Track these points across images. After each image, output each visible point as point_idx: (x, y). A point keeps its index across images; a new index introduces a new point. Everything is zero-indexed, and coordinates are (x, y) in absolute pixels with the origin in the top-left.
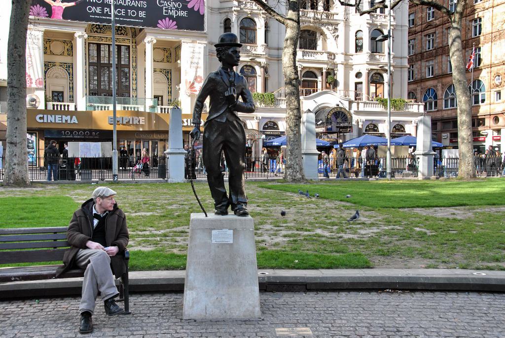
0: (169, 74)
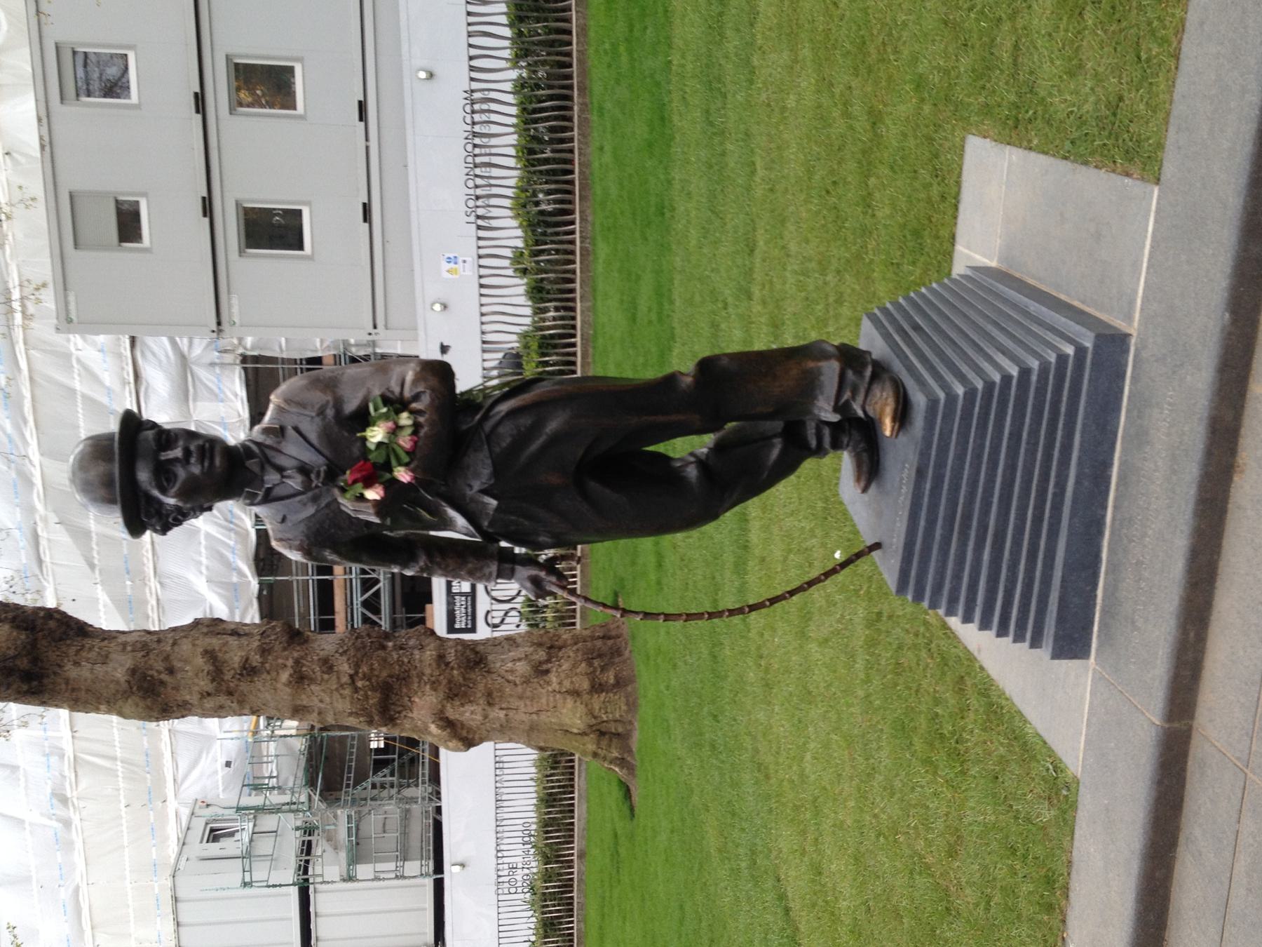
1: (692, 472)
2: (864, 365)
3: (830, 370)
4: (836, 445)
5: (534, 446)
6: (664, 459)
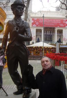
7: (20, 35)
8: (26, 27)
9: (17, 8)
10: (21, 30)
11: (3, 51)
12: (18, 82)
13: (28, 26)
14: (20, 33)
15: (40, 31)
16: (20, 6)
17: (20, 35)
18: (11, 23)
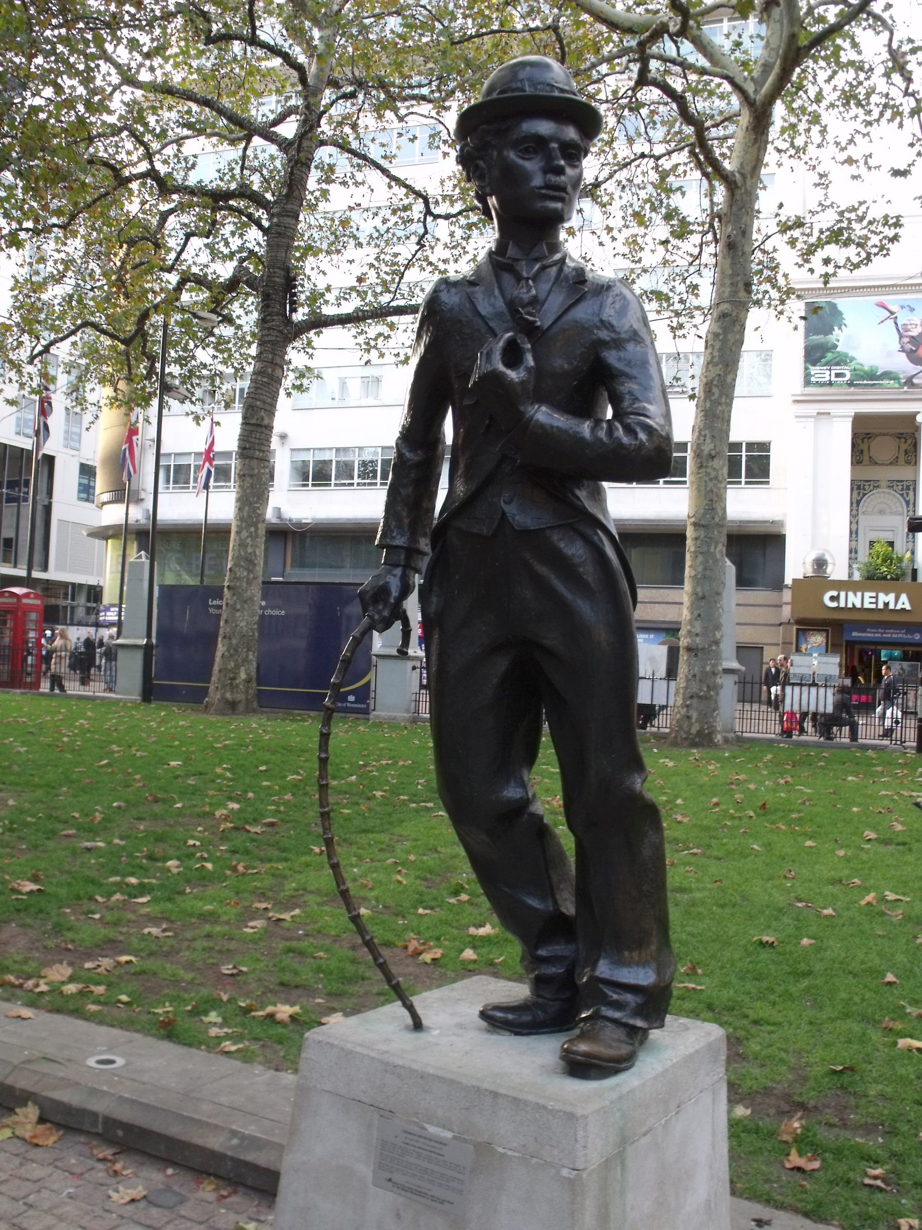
0: (911, 493)
1: (512, 793)
2: (646, 1017)
3: (644, 977)
4: (539, 983)
5: (542, 570)
6: (530, 758)
7: (543, 415)
8: (604, 335)
9: (515, 145)
10: (560, 363)
11: (395, 592)
12: (534, 902)
13: (637, 326)
14: (541, 401)
15: (900, 436)
16: (544, 127)
17: (543, 415)
18: (450, 299)
